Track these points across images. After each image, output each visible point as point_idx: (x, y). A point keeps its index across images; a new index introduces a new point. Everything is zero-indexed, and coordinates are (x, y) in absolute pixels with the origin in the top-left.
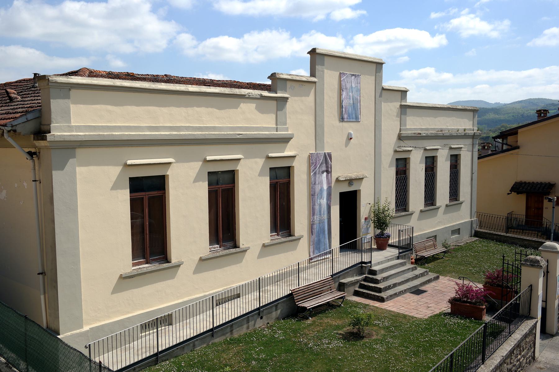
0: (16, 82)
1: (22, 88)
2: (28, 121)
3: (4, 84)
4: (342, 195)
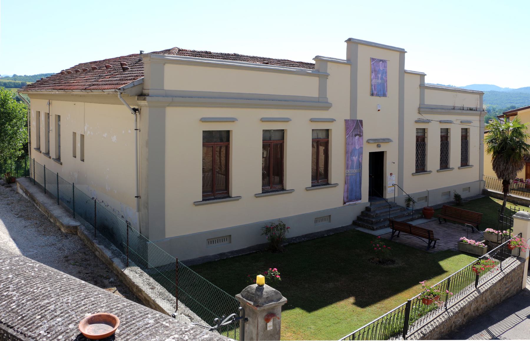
0: (127, 56)
1: (131, 61)
2: (134, 86)
3: (119, 57)
4: (371, 154)
